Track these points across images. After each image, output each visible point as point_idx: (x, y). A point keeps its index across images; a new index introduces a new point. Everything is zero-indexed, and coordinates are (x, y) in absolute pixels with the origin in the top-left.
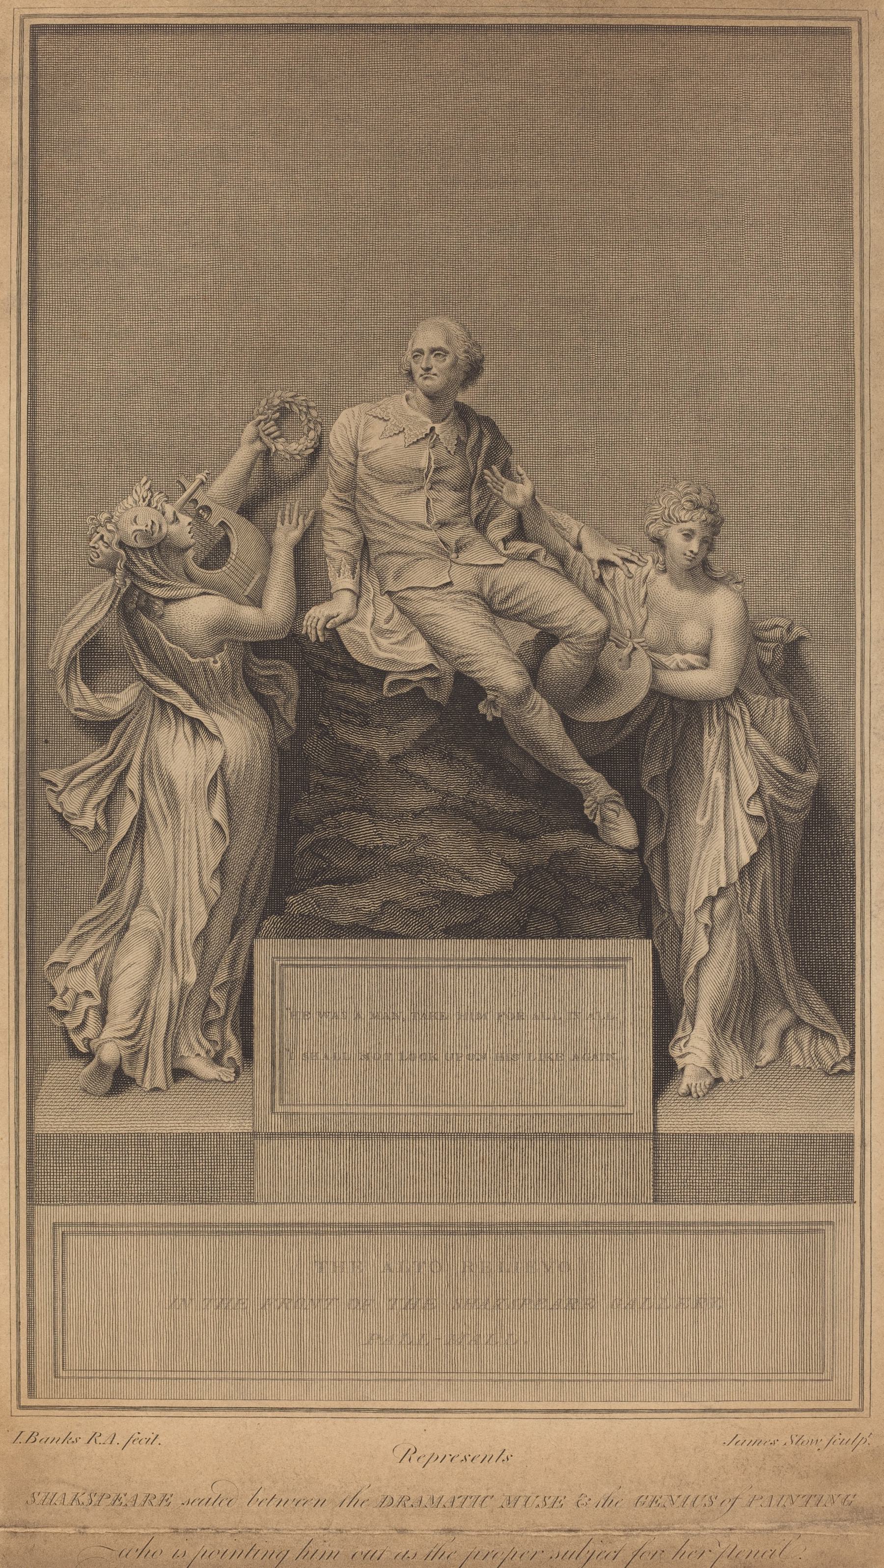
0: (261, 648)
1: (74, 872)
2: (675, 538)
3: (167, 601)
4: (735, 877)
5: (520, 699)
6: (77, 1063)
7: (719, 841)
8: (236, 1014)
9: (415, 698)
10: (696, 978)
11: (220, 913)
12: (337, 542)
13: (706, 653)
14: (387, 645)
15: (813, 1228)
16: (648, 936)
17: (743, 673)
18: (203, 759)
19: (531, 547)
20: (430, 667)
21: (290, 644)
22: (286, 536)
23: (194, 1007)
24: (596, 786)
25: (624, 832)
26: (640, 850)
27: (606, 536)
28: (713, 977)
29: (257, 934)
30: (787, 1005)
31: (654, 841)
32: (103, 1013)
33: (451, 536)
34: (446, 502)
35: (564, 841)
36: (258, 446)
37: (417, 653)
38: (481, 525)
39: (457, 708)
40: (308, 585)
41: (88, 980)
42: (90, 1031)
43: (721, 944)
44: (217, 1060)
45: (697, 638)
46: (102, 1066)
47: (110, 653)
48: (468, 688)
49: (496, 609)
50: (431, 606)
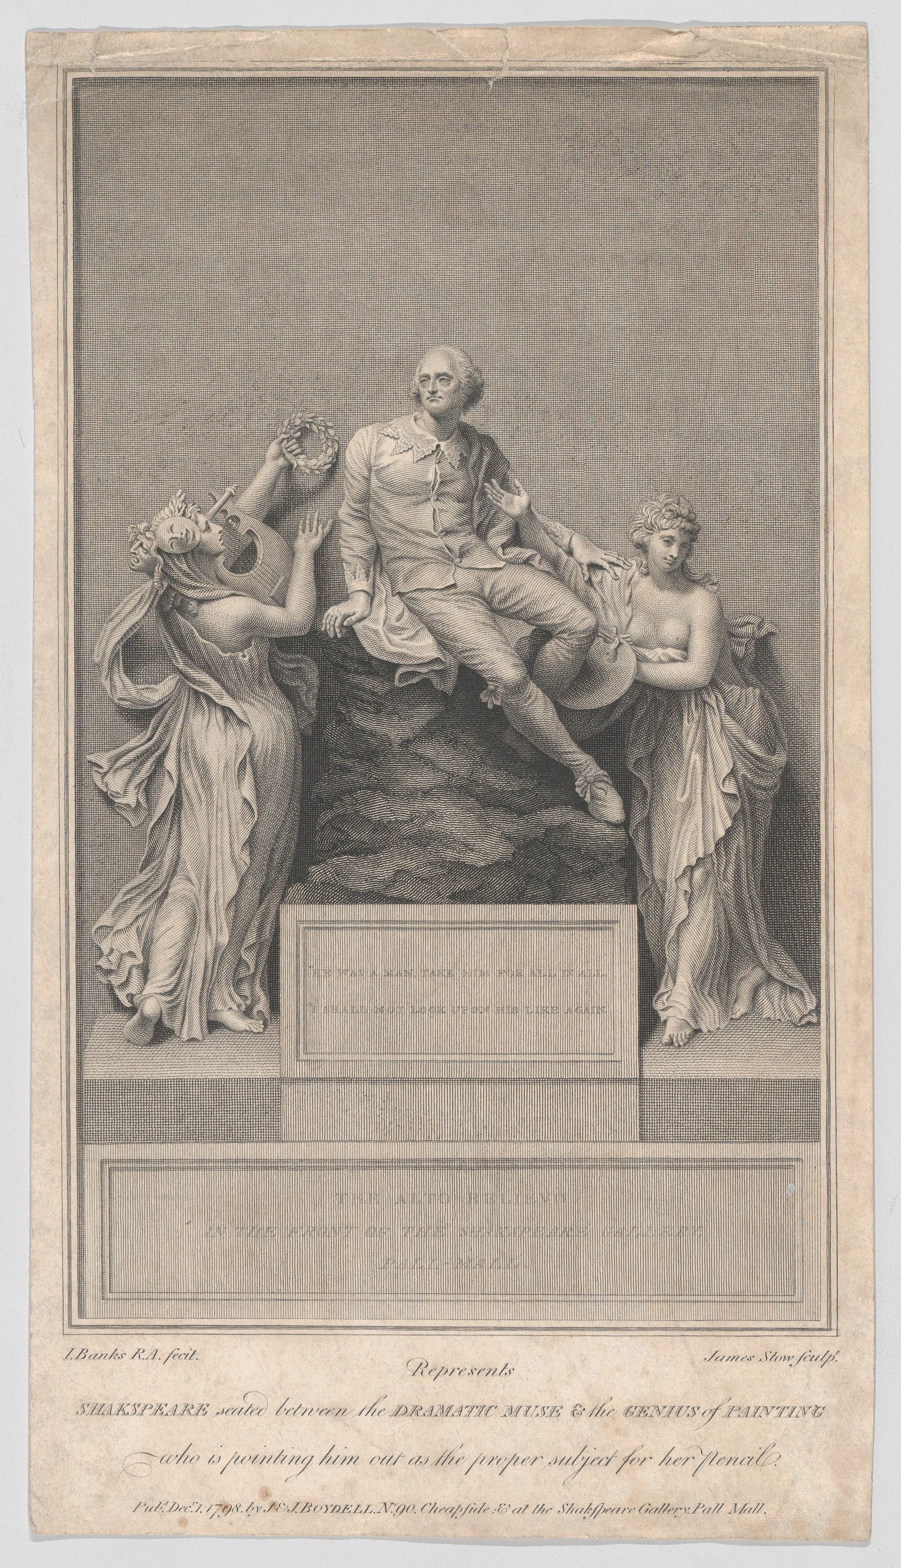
0: (283, 644)
1: (114, 845)
2: (657, 544)
3: (201, 602)
4: (712, 849)
5: (517, 689)
7: (696, 816)
8: (264, 971)
9: (422, 688)
11: (250, 882)
12: (353, 546)
13: (685, 647)
15: (784, 1165)
16: (634, 901)
18: (232, 745)
20: (437, 660)
21: (311, 641)
22: (307, 543)
24: (586, 766)
25: (612, 807)
26: (625, 824)
27: (593, 539)
28: (694, 936)
29: (280, 903)
31: (638, 817)
32: (145, 971)
33: (456, 542)
35: (555, 816)
36: (281, 462)
39: (460, 698)
40: (327, 587)
42: (133, 988)
44: (247, 1013)
45: (669, 635)
46: (144, 1019)
47: (136, 655)
48: (471, 679)
49: (498, 610)
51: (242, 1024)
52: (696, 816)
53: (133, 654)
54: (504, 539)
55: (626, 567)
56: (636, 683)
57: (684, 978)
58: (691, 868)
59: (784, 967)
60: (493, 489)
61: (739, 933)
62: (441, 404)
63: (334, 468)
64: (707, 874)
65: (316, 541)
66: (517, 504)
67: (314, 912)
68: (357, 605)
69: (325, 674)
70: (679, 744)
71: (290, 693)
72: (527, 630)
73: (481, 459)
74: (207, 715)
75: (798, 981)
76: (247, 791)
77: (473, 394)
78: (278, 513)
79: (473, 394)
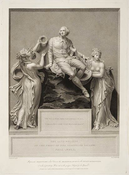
0: (40, 71)
1: (15, 96)
2: (95, 56)
3: (27, 64)
4: (103, 101)
5: (74, 77)
6: (14, 126)
7: (100, 97)
8: (34, 120)
9: (59, 78)
10: (98, 114)
11: (33, 106)
12: (50, 56)
13: (99, 71)
14: (56, 70)
15: (115, 137)
16: (91, 108)
17: (104, 75)
18: (32, 85)
19: (75, 57)
20: (61, 73)
21: (43, 70)
22: (43, 55)
23: (30, 118)
24: (84, 90)
25: (88, 95)
26: (90, 97)
27: (86, 55)
28: (99, 117)
29: (38, 108)
30: (109, 118)
31: (92, 96)
32: (17, 118)
33: (65, 56)
34: (64, 52)
35: (79, 97)
36: (40, 43)
37: (60, 71)
38: (69, 54)
39: (65, 80)
40: (46, 62)
41: (15, 114)
42: (16, 121)
43: (101, 110)
44: (33, 125)
45: (97, 69)
46: (17, 126)
47: (17, 73)
48: (67, 76)
49: (72, 65)
50: (62, 64)
51: (32, 127)
53: (16, 71)
54: (72, 55)
55: (90, 59)
56: (91, 77)
57: (98, 120)
58: (100, 104)
60: (71, 48)
61: (106, 113)
62: (63, 35)
63: (47, 44)
64: (102, 105)
65: (44, 55)
66: (74, 50)
68: (50, 65)
69: (45, 73)
70: (98, 87)
71: (40, 77)
75: (116, 121)
76: (33, 92)
77: (67, 34)
78: (39, 51)
79: (67, 34)
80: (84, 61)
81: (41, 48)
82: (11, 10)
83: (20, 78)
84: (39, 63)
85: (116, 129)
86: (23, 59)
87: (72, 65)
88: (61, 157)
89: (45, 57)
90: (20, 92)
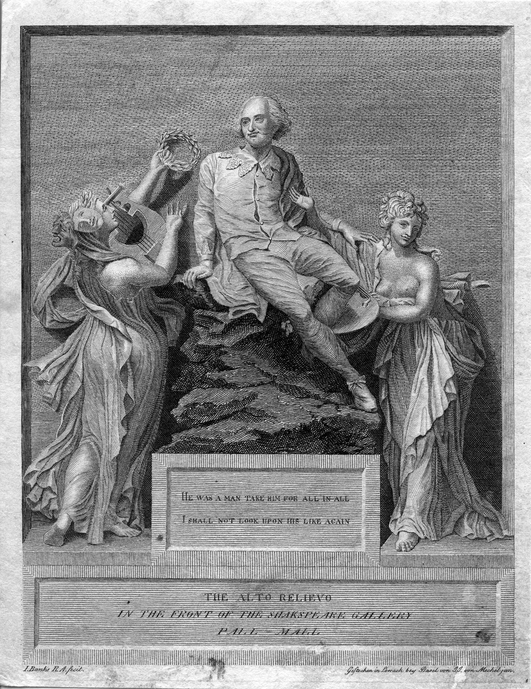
1: (49, 414)
2: (397, 229)
7: (425, 399)
8: (138, 505)
13: (413, 294)
18: (114, 349)
28: (417, 485)
39: (275, 337)
45: (403, 285)
46: (57, 530)
48: (277, 313)
49: (303, 267)
52: (425, 399)
59: (485, 506)
67: (185, 459)
68: (200, 269)
69: (175, 303)
72: (312, 281)
73: (288, 175)
74: (104, 331)
78: (158, 202)
79: (278, 131)
80: (351, 250)
81: (173, 187)
82: (23, 28)
83: (75, 319)
84: (151, 259)
85: (502, 549)
86: (84, 242)
87: (303, 267)
88: (20, 282)
89: (184, 232)
90: (73, 384)
